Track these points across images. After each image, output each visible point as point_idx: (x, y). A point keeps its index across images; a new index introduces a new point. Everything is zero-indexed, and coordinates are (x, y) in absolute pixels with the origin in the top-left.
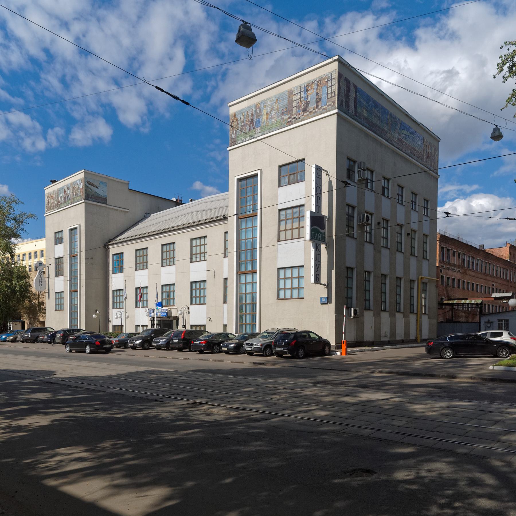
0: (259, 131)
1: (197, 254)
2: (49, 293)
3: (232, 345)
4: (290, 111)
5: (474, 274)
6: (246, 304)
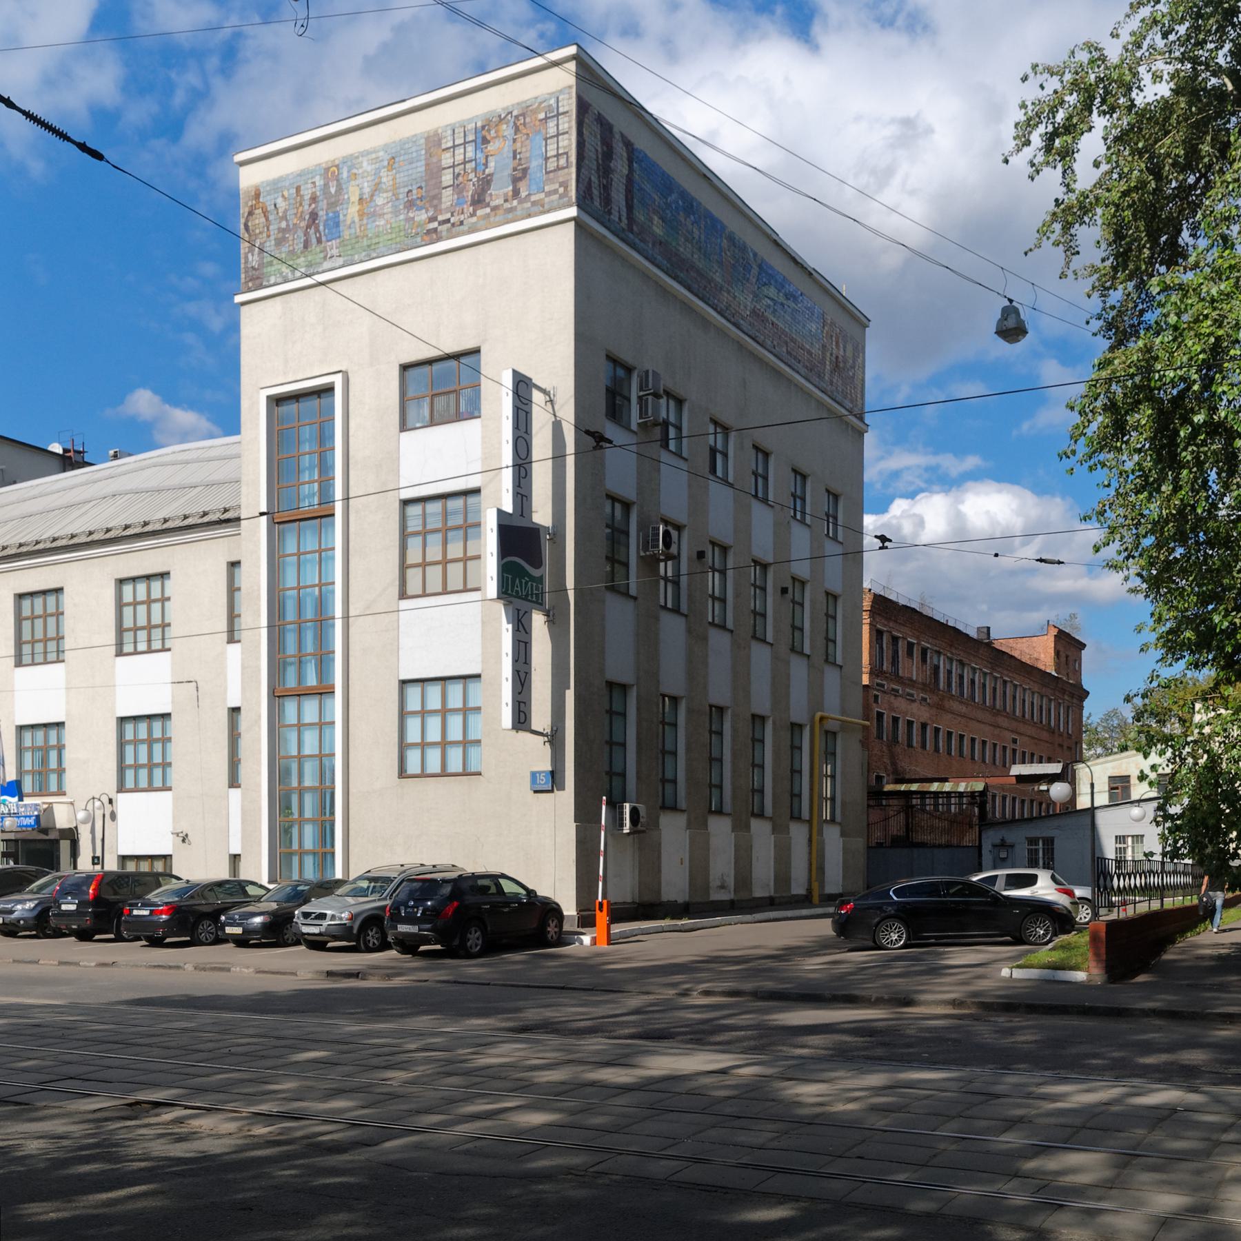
0: (335, 252)
1: (138, 631)
3: (258, 920)
4: (433, 200)
5: (963, 709)
6: (301, 791)
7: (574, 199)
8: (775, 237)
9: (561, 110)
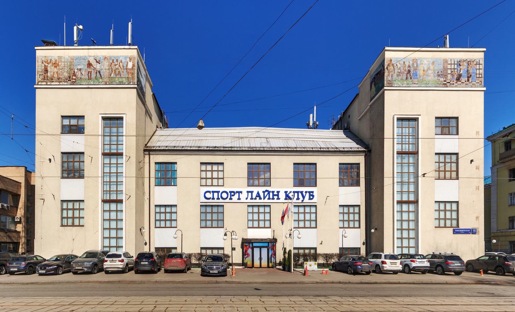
4: (446, 76)
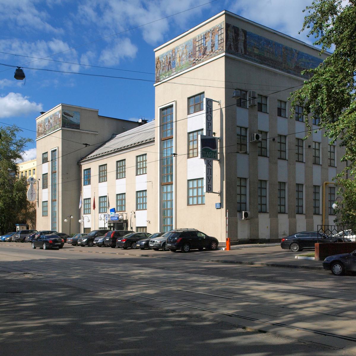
0: (174, 71)
1: (140, 169)
2: (38, 202)
3: (144, 242)
4: (194, 55)
6: (167, 209)
7: (225, 51)
8: (304, 44)
9: (222, 28)
